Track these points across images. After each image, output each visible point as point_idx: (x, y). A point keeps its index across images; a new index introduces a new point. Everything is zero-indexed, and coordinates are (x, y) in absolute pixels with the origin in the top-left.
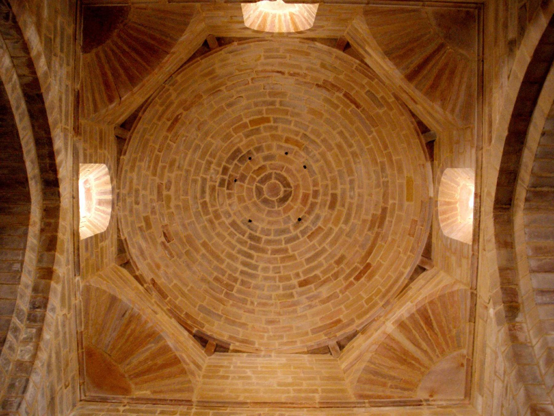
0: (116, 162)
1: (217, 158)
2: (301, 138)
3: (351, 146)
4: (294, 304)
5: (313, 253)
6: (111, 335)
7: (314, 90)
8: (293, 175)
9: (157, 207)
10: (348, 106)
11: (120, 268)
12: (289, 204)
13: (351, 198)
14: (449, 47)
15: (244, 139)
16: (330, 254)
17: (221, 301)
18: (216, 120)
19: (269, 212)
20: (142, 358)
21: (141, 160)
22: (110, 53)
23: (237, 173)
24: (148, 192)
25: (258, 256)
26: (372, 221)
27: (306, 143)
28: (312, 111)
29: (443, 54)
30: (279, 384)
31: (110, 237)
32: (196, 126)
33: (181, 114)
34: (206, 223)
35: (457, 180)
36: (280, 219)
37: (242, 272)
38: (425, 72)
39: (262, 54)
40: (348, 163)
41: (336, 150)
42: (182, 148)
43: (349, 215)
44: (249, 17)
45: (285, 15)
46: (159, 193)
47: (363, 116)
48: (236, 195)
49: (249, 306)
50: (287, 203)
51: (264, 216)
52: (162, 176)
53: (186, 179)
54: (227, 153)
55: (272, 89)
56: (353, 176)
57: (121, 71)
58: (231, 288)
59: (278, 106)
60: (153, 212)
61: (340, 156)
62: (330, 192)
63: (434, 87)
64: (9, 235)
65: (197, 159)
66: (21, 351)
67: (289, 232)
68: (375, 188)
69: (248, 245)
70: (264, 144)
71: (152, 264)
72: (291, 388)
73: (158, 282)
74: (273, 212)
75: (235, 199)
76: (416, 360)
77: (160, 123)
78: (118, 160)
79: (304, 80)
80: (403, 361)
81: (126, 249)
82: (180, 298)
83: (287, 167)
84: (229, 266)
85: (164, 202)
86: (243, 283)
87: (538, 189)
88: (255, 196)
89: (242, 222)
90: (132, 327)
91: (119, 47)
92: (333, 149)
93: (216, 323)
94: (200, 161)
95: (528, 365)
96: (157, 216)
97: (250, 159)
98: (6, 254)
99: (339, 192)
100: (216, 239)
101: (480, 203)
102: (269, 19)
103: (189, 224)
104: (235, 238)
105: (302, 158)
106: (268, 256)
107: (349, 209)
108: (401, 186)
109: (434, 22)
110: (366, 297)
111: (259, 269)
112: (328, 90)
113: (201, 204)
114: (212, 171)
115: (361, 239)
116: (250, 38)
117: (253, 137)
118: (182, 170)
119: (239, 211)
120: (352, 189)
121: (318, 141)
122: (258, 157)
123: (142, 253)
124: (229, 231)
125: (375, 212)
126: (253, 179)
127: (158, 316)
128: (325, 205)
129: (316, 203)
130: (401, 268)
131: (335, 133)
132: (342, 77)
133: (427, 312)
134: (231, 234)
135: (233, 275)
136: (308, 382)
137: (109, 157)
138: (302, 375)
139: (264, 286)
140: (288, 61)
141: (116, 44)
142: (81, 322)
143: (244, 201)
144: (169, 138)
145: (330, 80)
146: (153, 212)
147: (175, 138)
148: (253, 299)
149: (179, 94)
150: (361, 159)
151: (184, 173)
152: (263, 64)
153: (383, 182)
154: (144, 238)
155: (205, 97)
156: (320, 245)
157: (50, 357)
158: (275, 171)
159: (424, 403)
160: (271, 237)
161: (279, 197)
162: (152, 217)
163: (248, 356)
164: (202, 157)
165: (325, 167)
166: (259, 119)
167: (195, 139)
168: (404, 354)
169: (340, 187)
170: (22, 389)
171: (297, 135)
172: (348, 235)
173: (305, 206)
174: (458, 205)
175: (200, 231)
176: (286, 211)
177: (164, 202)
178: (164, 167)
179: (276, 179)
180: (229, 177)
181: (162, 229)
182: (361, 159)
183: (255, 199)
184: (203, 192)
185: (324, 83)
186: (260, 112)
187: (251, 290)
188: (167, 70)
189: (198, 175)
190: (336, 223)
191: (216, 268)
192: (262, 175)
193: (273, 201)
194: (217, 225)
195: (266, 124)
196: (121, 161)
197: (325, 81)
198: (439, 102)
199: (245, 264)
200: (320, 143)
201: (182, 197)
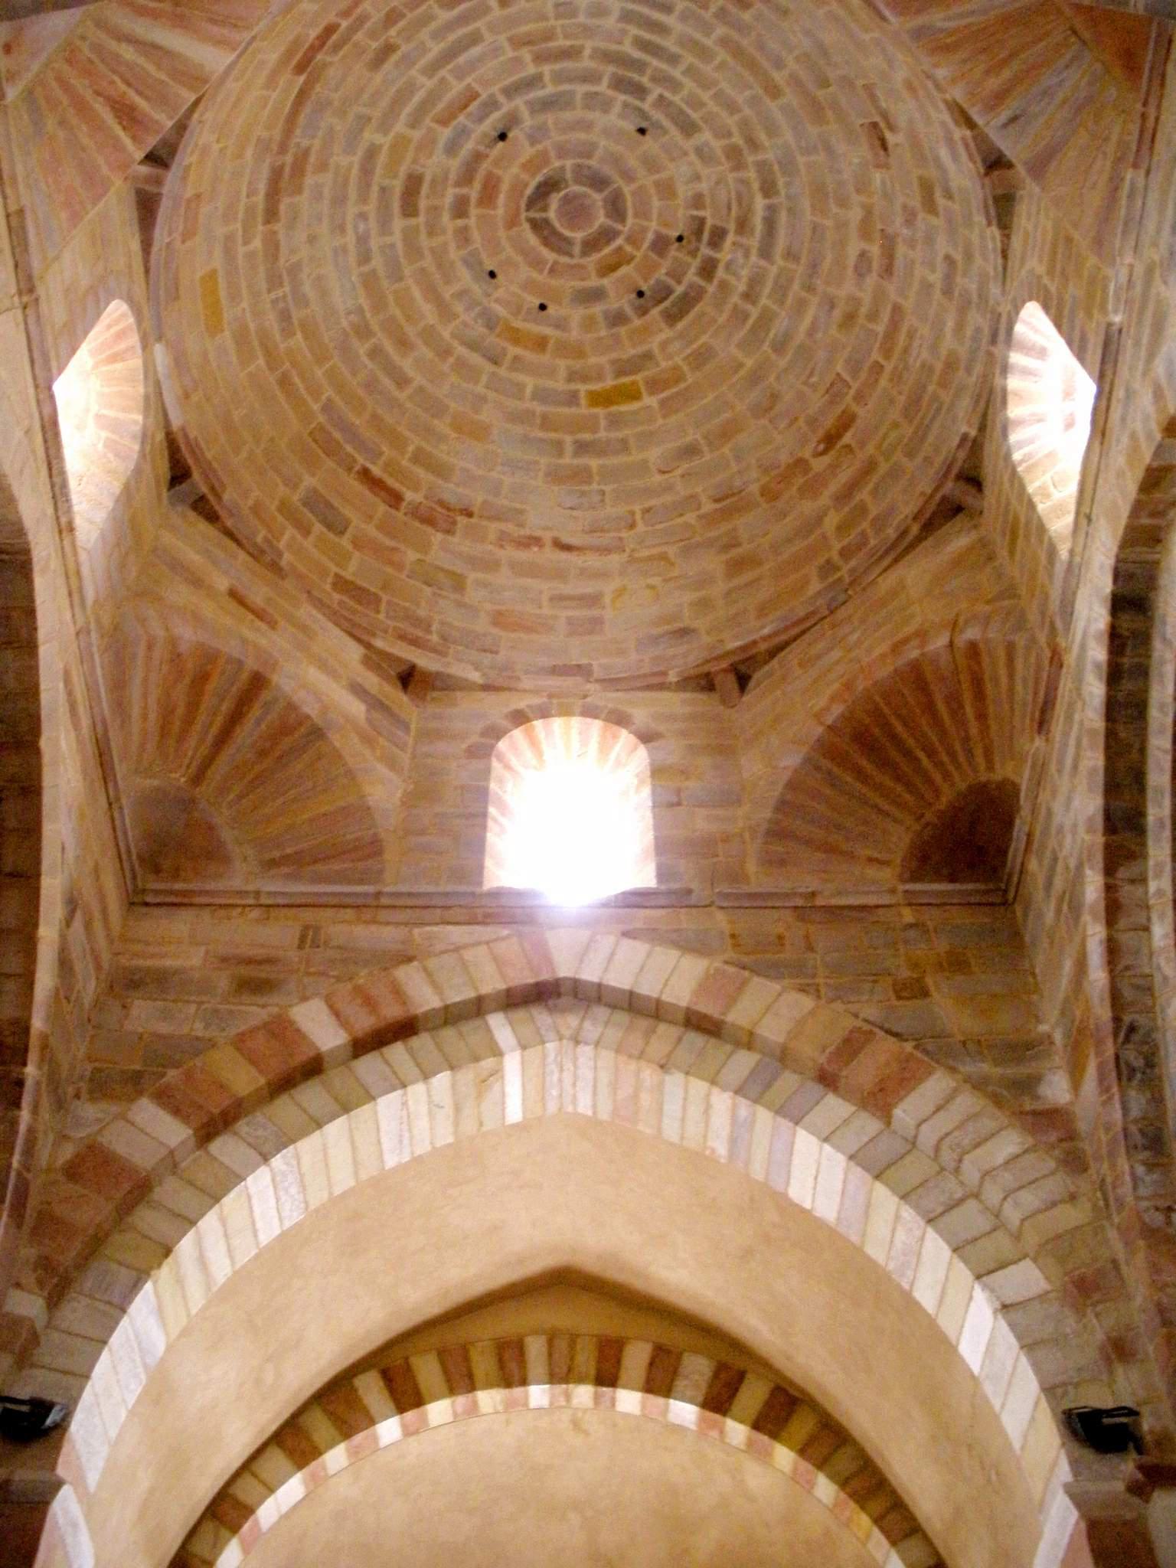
0: (989, 423)
1: (728, 307)
3: (376, 353)
5: (461, 59)
6: (1060, 84)
7: (477, 498)
8: (525, 252)
9: (899, 220)
12: (533, 175)
14: (183, 780)
15: (656, 351)
16: (414, 64)
18: (728, 415)
19: (589, 155)
21: (927, 369)
22: (962, 758)
23: (676, 259)
24: (919, 271)
27: (492, 340)
28: (479, 432)
32: (779, 407)
34: (767, 144)
36: (557, 137)
38: (226, 707)
39: (608, 614)
40: (379, 305)
41: (411, 332)
42: (821, 355)
43: (367, 171)
46: (889, 254)
47: (349, 449)
48: (680, 201)
51: (603, 143)
52: (879, 296)
53: (814, 266)
55: (583, 494)
56: (361, 275)
59: (568, 439)
60: (910, 219)
62: (421, 219)
63: (202, 678)
69: (649, 72)
70: (603, 333)
74: (581, 155)
75: (684, 191)
78: (982, 428)
79: (502, 526)
81: (990, 202)
83: (541, 271)
84: (707, 30)
85: (879, 226)
89: (665, 132)
91: (939, 765)
96: (900, 200)
99: (398, 224)
101: (58, 518)
105: (499, 299)
107: (368, 185)
109: (227, 835)
111: (616, 14)
112: (441, 503)
113: (777, 193)
114: (745, 273)
115: (329, 119)
117: (633, 352)
119: (673, 160)
120: (362, 240)
121: (461, 350)
126: (633, 240)
128: (433, 181)
129: (458, 184)
131: (419, 380)
132: (411, 556)
133: (134, 138)
134: (696, 103)
141: (947, 776)
142: (1131, 196)
143: (657, 184)
144: (852, 392)
146: (910, 219)
147: (835, 389)
150: (345, 323)
152: (603, 575)
155: (754, 488)
156: (443, 80)
158: (574, 261)
160: (581, 89)
161: (562, 193)
162: (916, 202)
164: (766, 319)
166: (617, 403)
167: (786, 370)
169: (397, 238)
171: (516, 359)
172: (364, 120)
176: (543, 158)
178: (873, 316)
179: (568, 241)
180: (697, 249)
182: (345, 323)
183: (627, 190)
184: (770, 224)
185: (454, 523)
186: (615, 422)
190: (399, 146)
192: (607, 250)
193: (578, 181)
194: (735, 130)
196: (976, 421)
198: (183, 648)
199: (661, 29)
200: (455, 344)
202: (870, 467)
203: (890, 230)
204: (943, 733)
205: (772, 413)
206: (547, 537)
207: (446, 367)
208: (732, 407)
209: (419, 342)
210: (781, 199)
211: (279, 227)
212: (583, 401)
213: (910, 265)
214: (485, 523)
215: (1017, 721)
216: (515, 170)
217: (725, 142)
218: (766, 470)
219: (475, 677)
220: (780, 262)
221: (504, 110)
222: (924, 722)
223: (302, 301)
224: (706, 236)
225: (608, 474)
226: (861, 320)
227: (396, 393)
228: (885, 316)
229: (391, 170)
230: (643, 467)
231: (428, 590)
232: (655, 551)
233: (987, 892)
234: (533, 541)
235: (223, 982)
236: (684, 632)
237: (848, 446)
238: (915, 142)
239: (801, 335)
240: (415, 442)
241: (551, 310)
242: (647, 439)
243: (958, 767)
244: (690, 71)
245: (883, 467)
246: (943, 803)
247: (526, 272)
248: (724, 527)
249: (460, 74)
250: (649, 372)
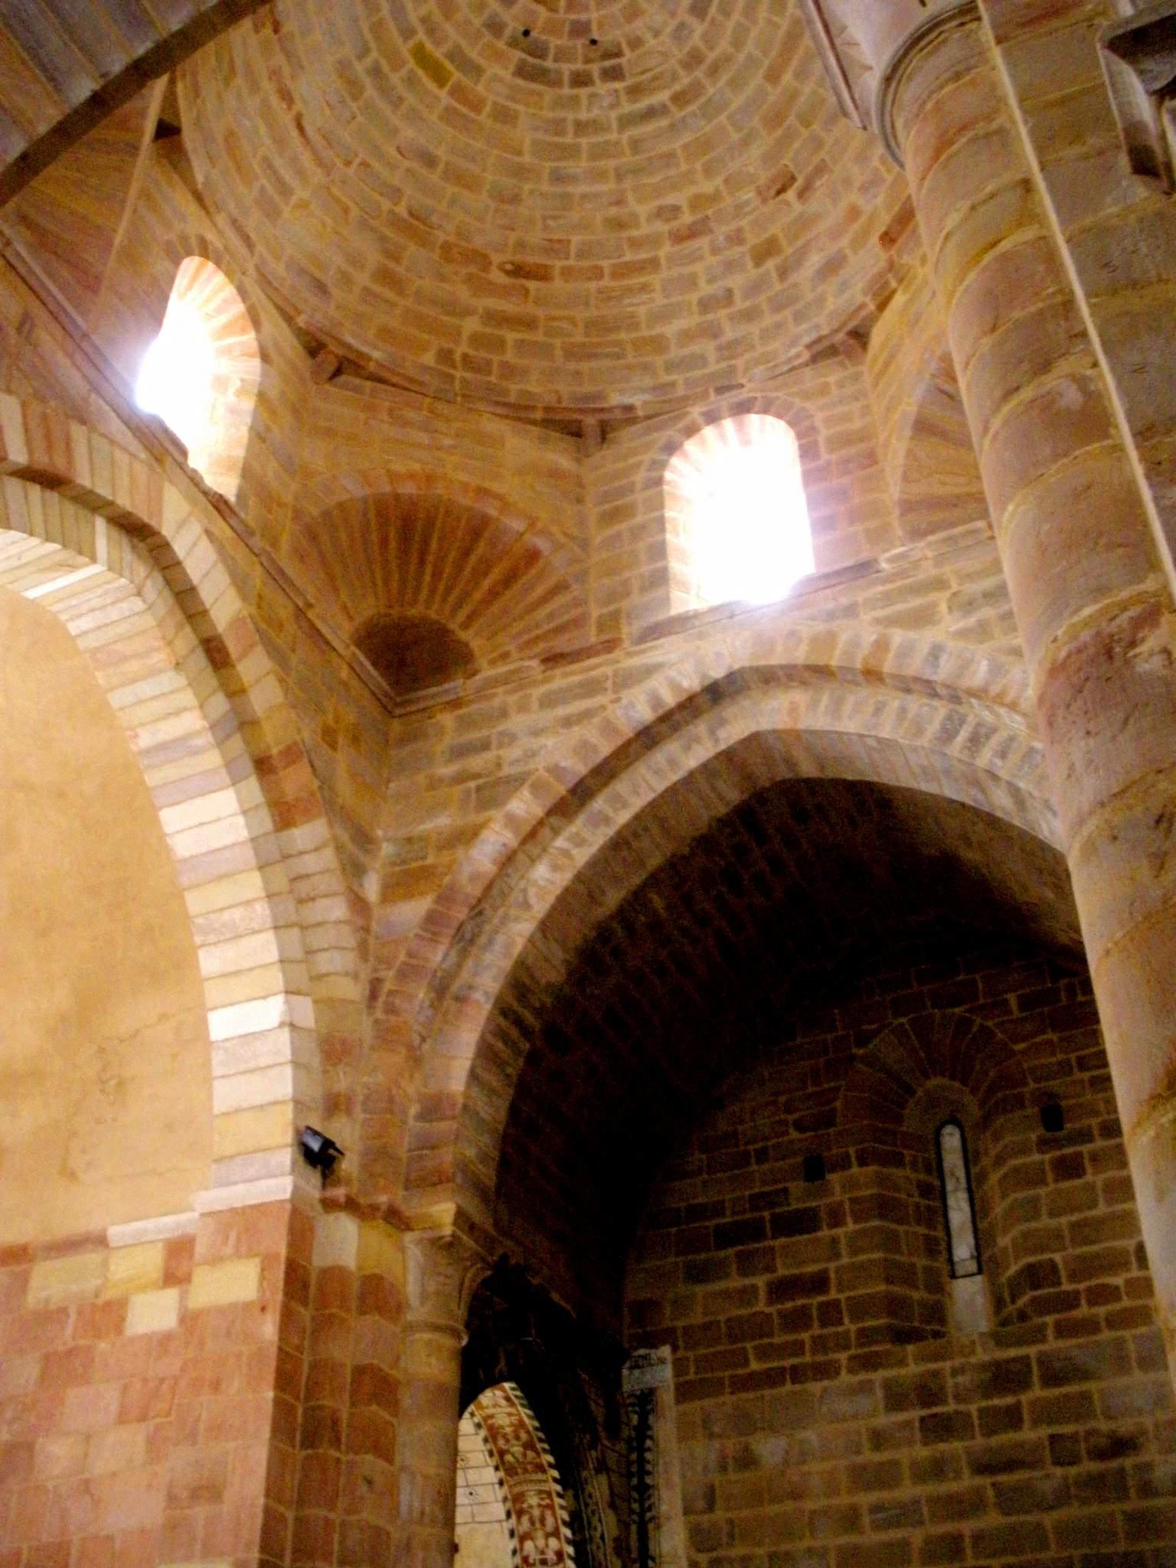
1: (560, 114)
22: (452, 599)
23: (575, 47)
24: (698, 268)
33: (501, 268)
46: (693, 232)
48: (627, 28)
52: (654, 241)
54: (540, 95)
55: (343, 102)
57: (473, 559)
60: (737, 238)
65: (584, 164)
75: (638, 27)
85: (710, 212)
91: (433, 591)
94: (584, 155)
97: (526, 33)
100: (750, 47)
102: (223, 319)
103: (739, 129)
114: (596, 112)
146: (737, 238)
147: (557, 246)
151: (628, 183)
155: (441, 237)
162: (752, 239)
164: (572, 152)
177: (710, 212)
178: (635, 244)
181: (771, 202)
184: (650, 114)
186: (411, 81)
195: (429, 46)
202: (530, 324)
204: (455, 578)
205: (506, 207)
206: (299, 106)
210: (678, 114)
212: (411, 43)
213: (695, 258)
214: (277, 48)
215: (519, 626)
217: (701, 45)
218: (459, 234)
219: (200, 178)
220: (625, 137)
224: (608, 63)
226: (625, 234)
228: (644, 255)
230: (394, 132)
233: (386, 695)
234: (287, 96)
236: (321, 288)
237: (527, 291)
238: (804, 223)
242: (414, 117)
243: (444, 600)
245: (539, 336)
246: (412, 612)
250: (466, 81)
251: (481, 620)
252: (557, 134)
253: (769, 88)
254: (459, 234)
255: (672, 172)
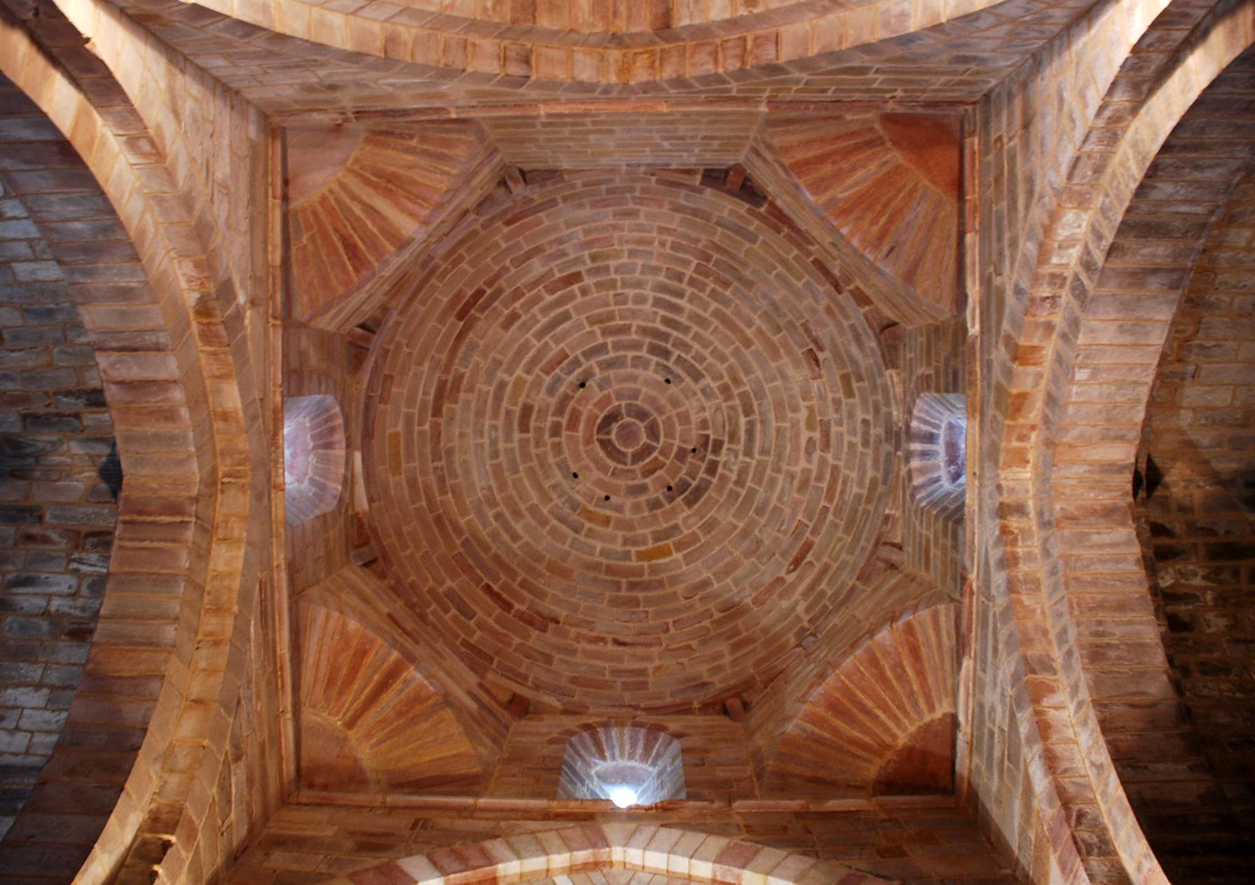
1: (726, 491)
2: (582, 525)
3: (498, 516)
4: (589, 244)
5: (559, 329)
6: (916, 216)
8: (596, 461)
9: (831, 410)
10: (505, 587)
11: (897, 320)
12: (602, 410)
13: (494, 427)
16: (529, 330)
17: (718, 248)
18: (729, 558)
20: (860, 174)
21: (858, 497)
22: (908, 707)
24: (847, 438)
25: (654, 321)
26: (458, 391)
27: (574, 517)
29: (348, 710)
30: (611, 132)
31: (914, 378)
33: (789, 572)
34: (745, 380)
35: (314, 490)
36: (616, 386)
37: (680, 294)
40: (502, 486)
41: (523, 507)
43: (498, 398)
44: (674, 759)
45: (614, 758)
46: (826, 435)
47: (478, 571)
48: (693, 426)
49: (669, 239)
50: (605, 413)
51: (644, 390)
52: (823, 462)
54: (710, 498)
55: (633, 613)
57: (889, 674)
58: (699, 269)
59: (624, 581)
61: (517, 498)
62: (531, 435)
64: (1095, 426)
66: (1080, 226)
67: (600, 364)
68: (453, 448)
71: (840, 317)
72: (590, 127)
73: (828, 286)
74: (630, 398)
75: (695, 418)
76: (368, 182)
77: (825, 559)
80: (391, 178)
82: (790, 257)
84: (705, 306)
85: (819, 418)
86: (679, 277)
87: (178, 519)
88: (660, 423)
89: (682, 380)
90: (875, 229)
92: (528, 509)
93: (725, 214)
94: (756, 487)
95: (172, 223)
96: (830, 396)
97: (670, 488)
98: (1101, 395)
99: (517, 436)
100: (727, 351)
104: (693, 353)
106: (635, 323)
108: (410, 456)
110: (464, 265)
111: (650, 301)
112: (539, 614)
113: (753, 412)
114: (735, 468)
115: (476, 358)
116: (673, 713)
117: (665, 525)
118: (788, 472)
120: (494, 442)
121: (555, 522)
122: (656, 491)
123: (858, 338)
124: (705, 364)
125: (454, 406)
127: (829, 239)
128: (539, 411)
130: (404, 320)
131: (526, 538)
134: (700, 359)
135: (696, 291)
136: (560, 136)
137: (913, 518)
138: (571, 144)
139: (642, 273)
140: (607, 665)
141: (898, 723)
143: (678, 415)
145: (535, 633)
146: (837, 403)
148: (662, 250)
149: (793, 609)
151: (785, 467)
153: (440, 459)
154: (854, 362)
156: (547, 343)
157: (1027, 207)
159: (351, 116)
160: (630, 354)
163: (668, 165)
164: (751, 494)
165: (541, 478)
168: (390, 190)
169: (515, 445)
170: (1081, 164)
171: (590, 530)
172: (497, 363)
173: (574, 410)
174: (311, 444)
175: (755, 365)
176: (607, 400)
178: (819, 478)
179: (624, 454)
180: (705, 456)
183: (660, 420)
184: (750, 433)
187: (665, 266)
188: (812, 666)
189: (759, 462)
190: (519, 383)
191: (726, 302)
193: (629, 415)
194: (725, 374)
195: (642, 548)
197: (544, 630)
200: (550, 517)
201: (787, 425)
202: (826, 569)
203: (826, 419)
207: (544, 532)
208: (731, 554)
209: (527, 514)
211: (442, 421)
212: (634, 558)
213: (840, 437)
216: (590, 407)
221: (584, 367)
222: (879, 689)
223: (454, 475)
225: (648, 601)
226: (812, 483)
227: (511, 544)
229: (513, 401)
231: (527, 661)
232: (684, 644)
235: (349, 844)
237: (810, 562)
239: (774, 501)
240: (522, 575)
241: (613, 499)
243: (906, 713)
244: (697, 337)
247: (597, 474)
248: (730, 626)
249: (557, 341)
251: (933, 693)
252: (737, 499)
253: (753, 347)
254: (756, 589)
255: (788, 434)
